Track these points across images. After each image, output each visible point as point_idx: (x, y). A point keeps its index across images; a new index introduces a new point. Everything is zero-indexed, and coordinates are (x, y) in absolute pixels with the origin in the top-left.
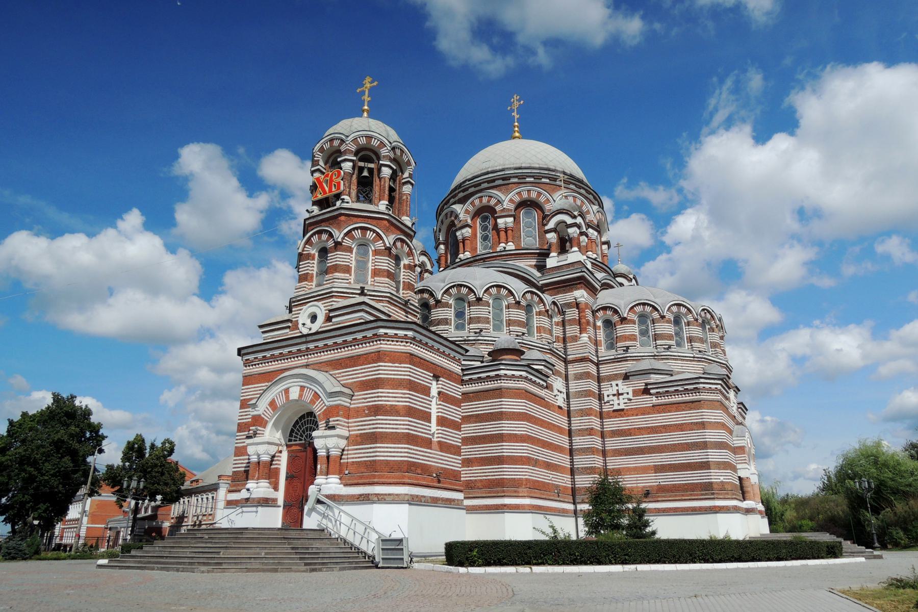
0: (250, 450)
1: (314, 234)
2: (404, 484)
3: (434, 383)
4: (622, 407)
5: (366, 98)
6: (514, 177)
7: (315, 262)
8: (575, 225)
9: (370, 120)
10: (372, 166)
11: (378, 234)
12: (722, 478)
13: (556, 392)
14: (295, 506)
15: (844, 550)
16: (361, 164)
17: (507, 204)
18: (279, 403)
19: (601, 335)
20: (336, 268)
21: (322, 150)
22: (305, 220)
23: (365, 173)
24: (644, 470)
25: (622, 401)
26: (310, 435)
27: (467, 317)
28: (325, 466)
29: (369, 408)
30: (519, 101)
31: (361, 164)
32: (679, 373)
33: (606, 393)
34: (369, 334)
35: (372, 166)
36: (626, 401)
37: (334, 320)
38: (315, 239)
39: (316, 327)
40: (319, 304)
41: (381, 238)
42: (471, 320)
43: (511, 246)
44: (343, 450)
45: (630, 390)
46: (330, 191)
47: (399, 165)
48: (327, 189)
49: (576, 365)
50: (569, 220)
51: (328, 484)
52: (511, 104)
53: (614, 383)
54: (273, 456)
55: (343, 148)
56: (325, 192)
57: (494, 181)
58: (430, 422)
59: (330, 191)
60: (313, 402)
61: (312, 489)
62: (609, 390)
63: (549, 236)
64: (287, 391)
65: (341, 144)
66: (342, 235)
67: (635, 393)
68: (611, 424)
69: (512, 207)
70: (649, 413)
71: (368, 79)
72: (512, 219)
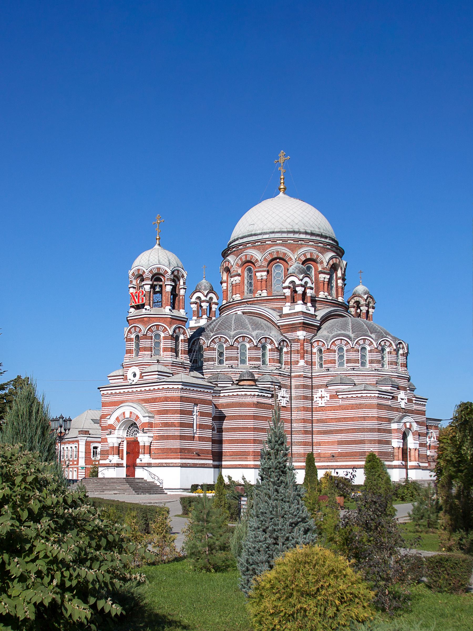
0: (109, 440)
2: (178, 458)
4: (323, 405)
6: (268, 241)
7: (134, 342)
10: (161, 283)
12: (319, 451)
14: (131, 467)
16: (155, 283)
18: (120, 418)
19: (316, 359)
21: (133, 274)
24: (332, 443)
25: (323, 402)
28: (143, 450)
29: (162, 423)
30: (285, 156)
33: (315, 396)
35: (161, 283)
36: (326, 401)
37: (144, 377)
39: (136, 379)
44: (151, 443)
45: (328, 395)
46: (139, 302)
47: (176, 278)
48: (137, 300)
51: (144, 458)
52: (278, 158)
53: (320, 390)
54: (120, 444)
56: (136, 303)
59: (139, 302)
60: (136, 420)
61: (138, 461)
62: (317, 396)
64: (124, 413)
68: (317, 415)
69: (265, 264)
71: (282, 153)
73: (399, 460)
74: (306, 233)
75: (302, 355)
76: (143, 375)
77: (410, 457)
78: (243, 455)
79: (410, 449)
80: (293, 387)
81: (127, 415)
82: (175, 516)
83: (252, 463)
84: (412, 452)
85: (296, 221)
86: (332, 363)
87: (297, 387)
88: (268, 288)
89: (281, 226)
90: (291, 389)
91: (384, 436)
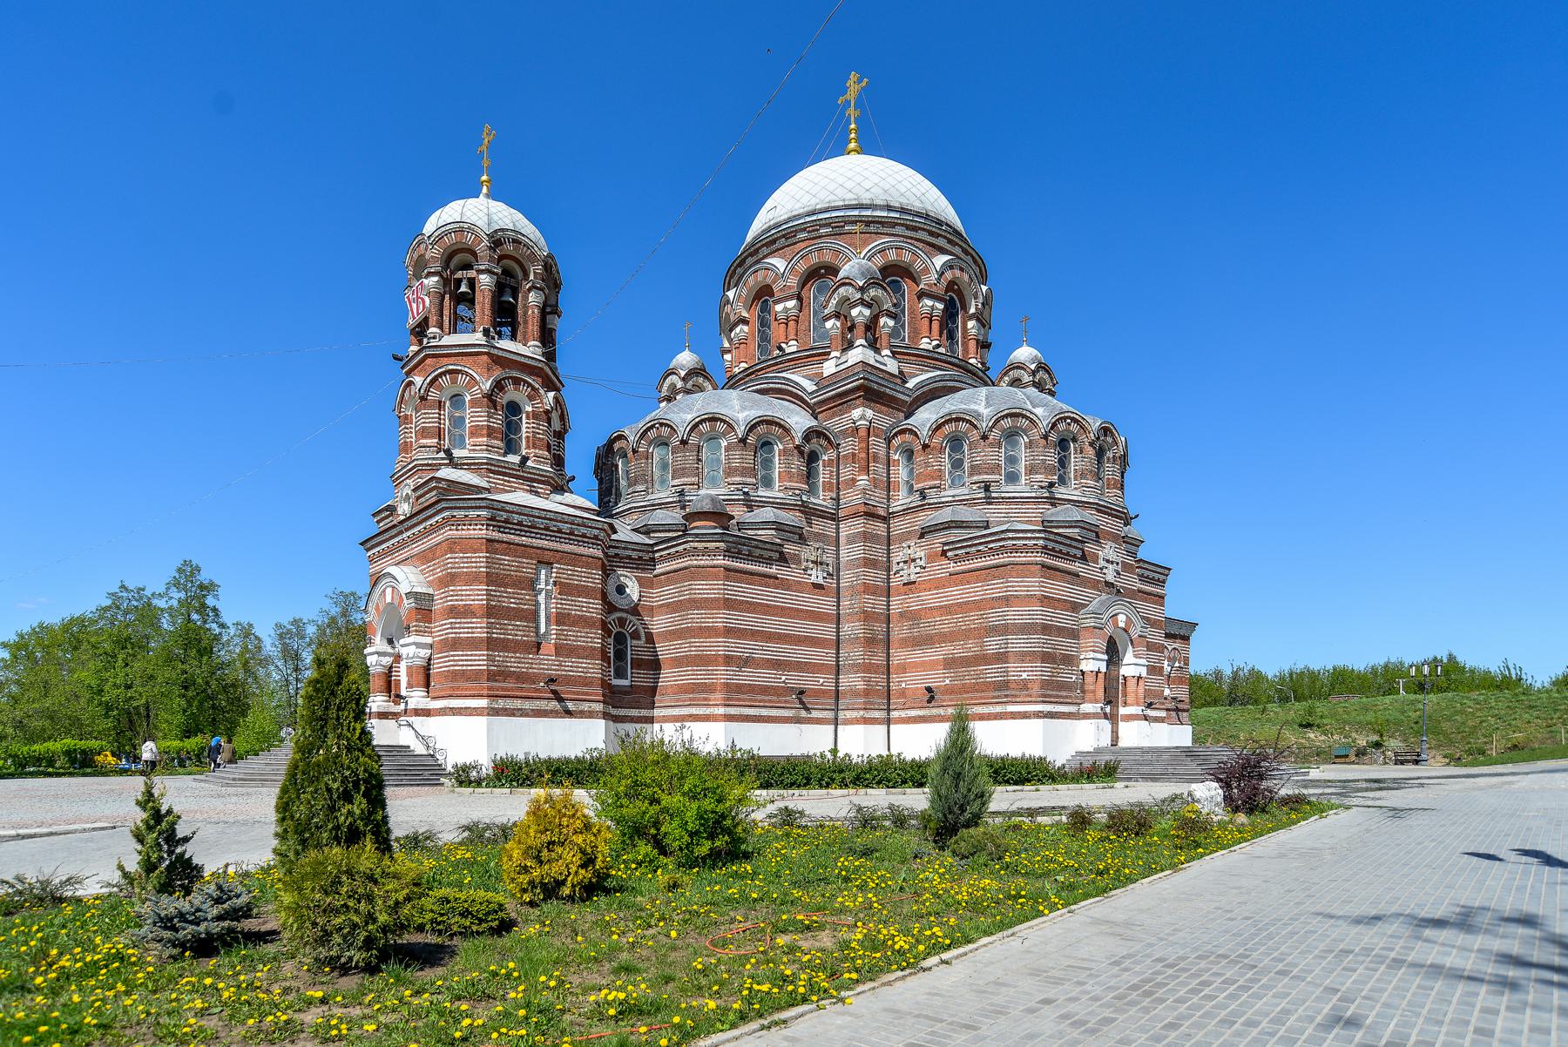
5: (852, 112)
9: (492, 203)
13: (1102, 563)
15: (885, 753)
23: (463, 289)
27: (966, 465)
30: (860, 81)
32: (1000, 523)
33: (894, 560)
42: (975, 470)
49: (849, 522)
52: (845, 90)
57: (774, 241)
62: (898, 556)
63: (829, 324)
67: (931, 558)
70: (944, 586)
71: (853, 76)
73: (1096, 702)
74: (889, 208)
75: (864, 463)
77: (1125, 695)
78: (698, 692)
79: (1125, 678)
80: (842, 540)
82: (1526, 853)
83: (721, 711)
84: (1131, 684)
85: (867, 185)
86: (934, 479)
87: (851, 540)
88: (801, 334)
89: (832, 197)
90: (838, 546)
91: (1064, 645)
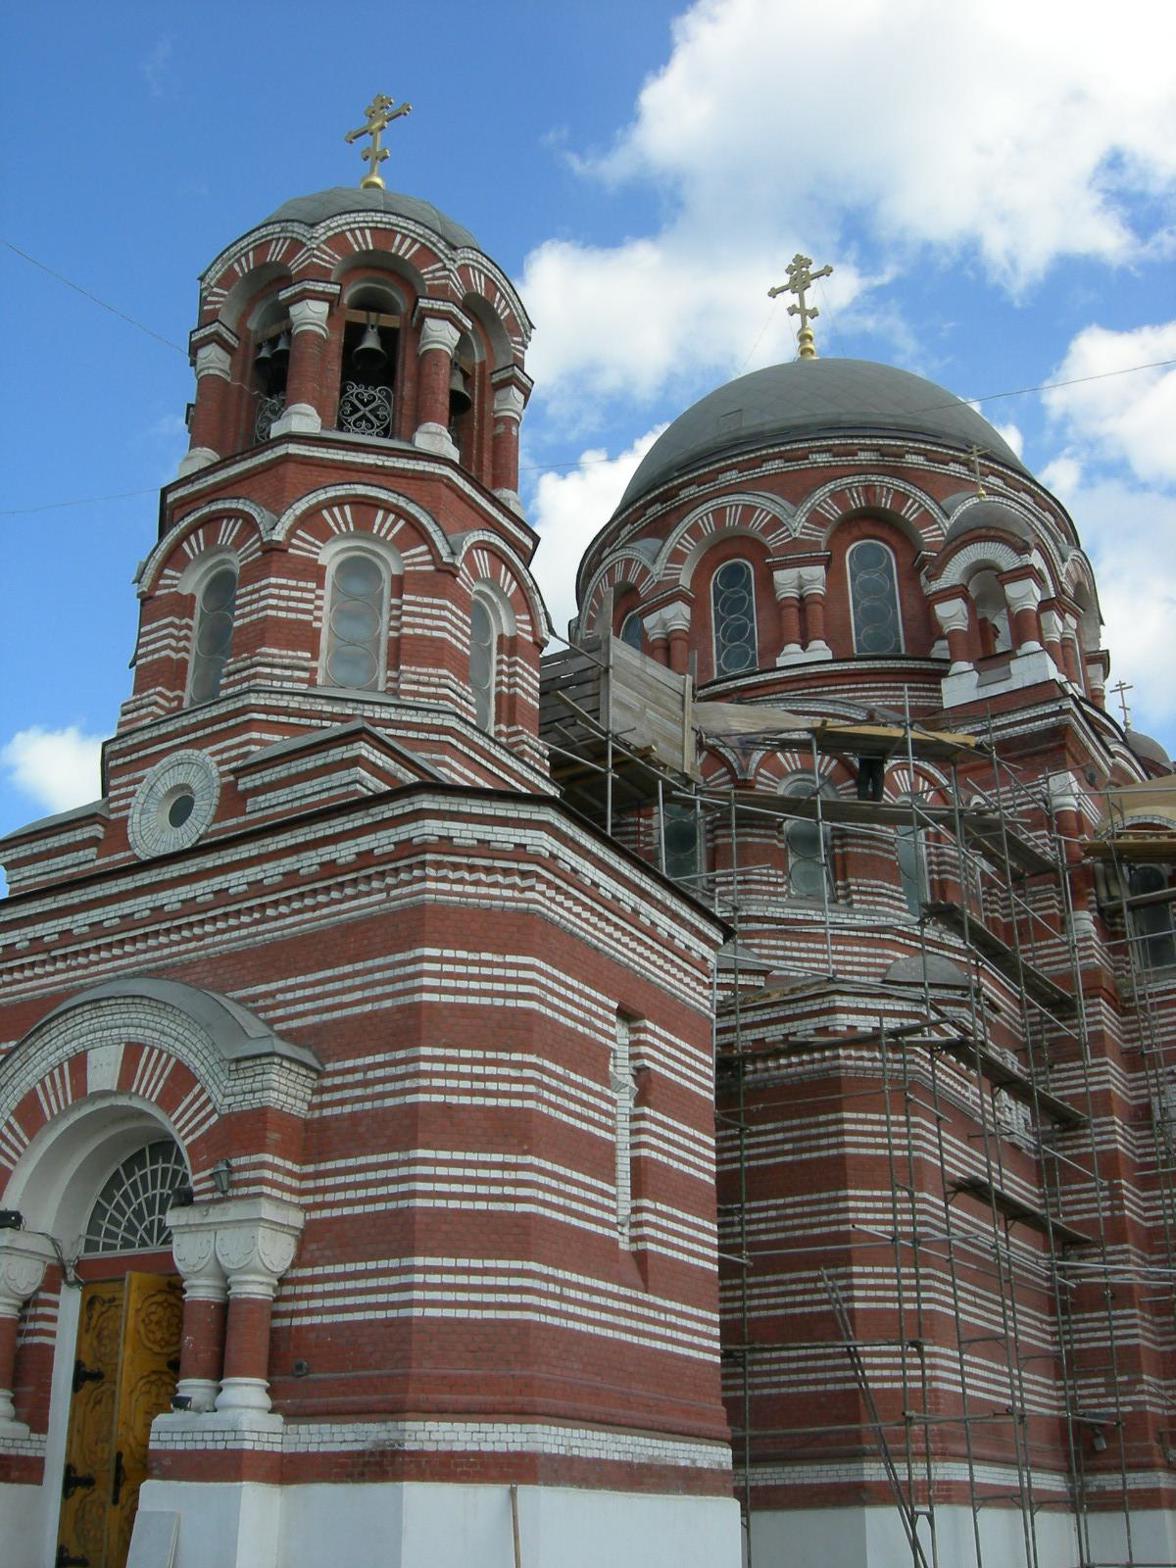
1: (192, 529)
3: (620, 1030)
8: (1026, 572)
11: (413, 524)
17: (798, 524)
20: (266, 631)
22: (165, 492)
23: (371, 342)
26: (162, 1228)
31: (360, 317)
34: (381, 842)
35: (390, 321)
38: (193, 547)
40: (203, 754)
41: (424, 537)
43: (820, 650)
50: (1007, 560)
54: (28, 1303)
55: (295, 266)
58: (612, 1180)
63: (943, 610)
64: (79, 1064)
65: (291, 253)
66: (287, 520)
69: (822, 536)
72: (819, 571)
76: (246, 783)
81: (104, 1072)
